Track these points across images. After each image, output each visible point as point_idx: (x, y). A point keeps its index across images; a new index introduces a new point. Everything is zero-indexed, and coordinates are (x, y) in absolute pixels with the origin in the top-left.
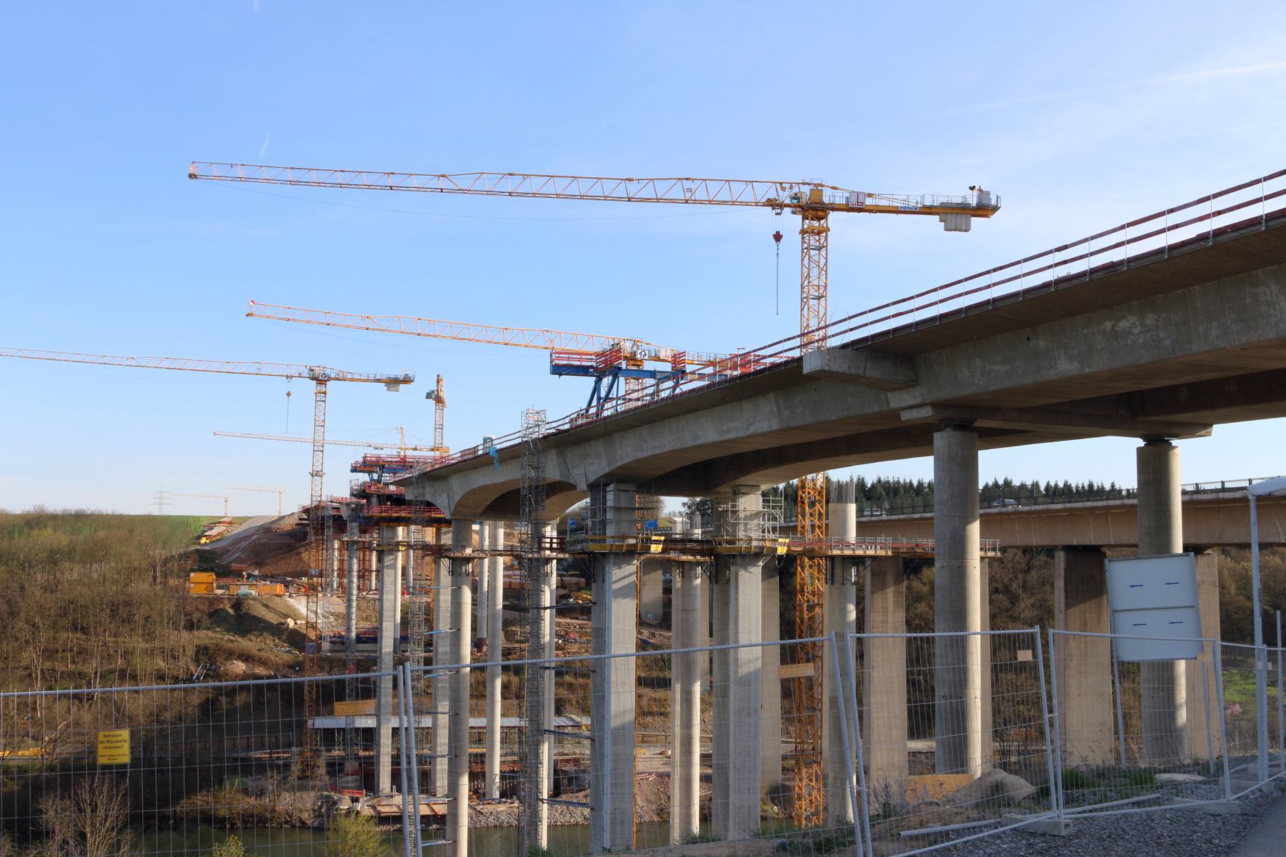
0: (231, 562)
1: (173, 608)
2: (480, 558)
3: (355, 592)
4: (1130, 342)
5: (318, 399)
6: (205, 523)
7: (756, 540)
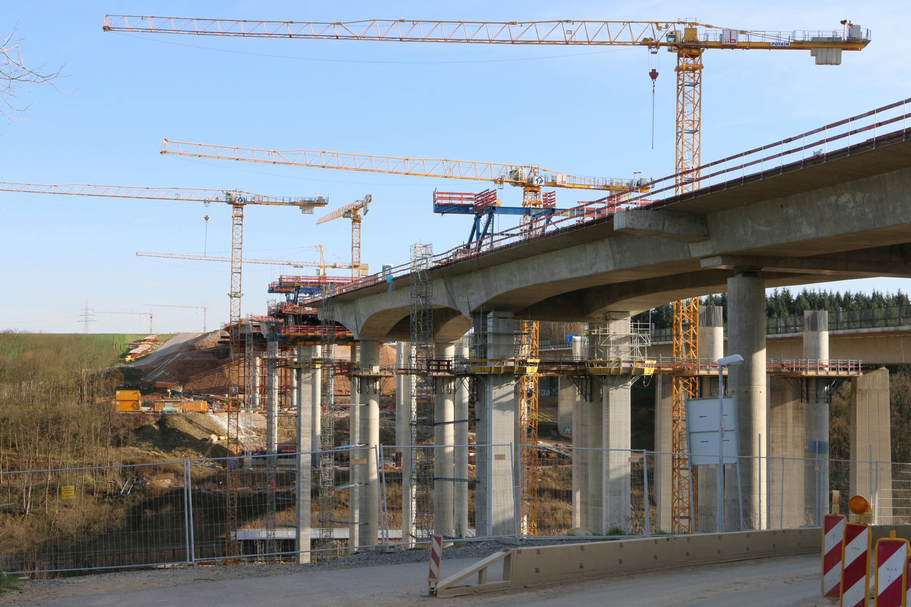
0: (156, 380)
1: (99, 426)
2: (387, 377)
3: (276, 409)
4: (847, 214)
5: (235, 222)
6: (130, 341)
7: (624, 362)
